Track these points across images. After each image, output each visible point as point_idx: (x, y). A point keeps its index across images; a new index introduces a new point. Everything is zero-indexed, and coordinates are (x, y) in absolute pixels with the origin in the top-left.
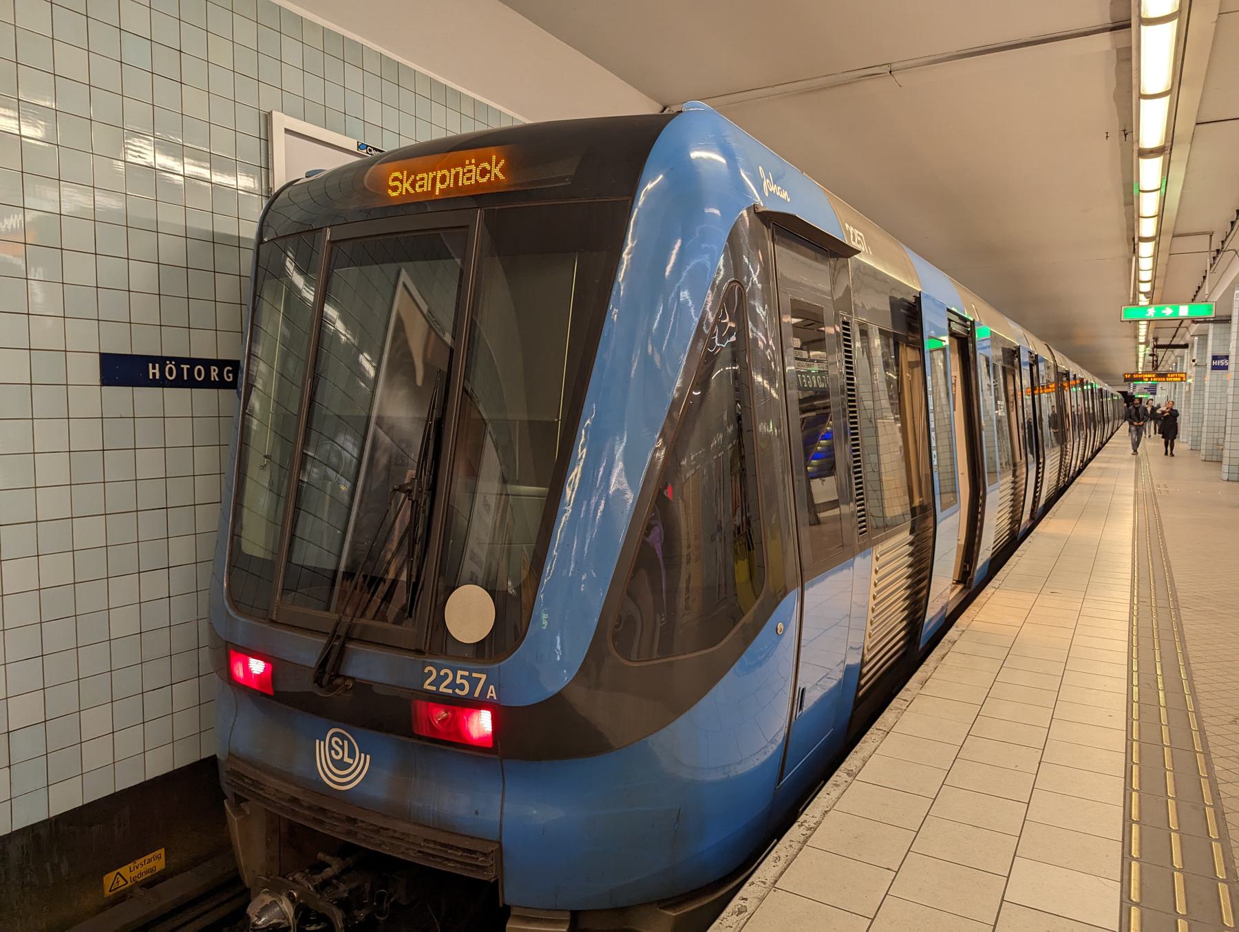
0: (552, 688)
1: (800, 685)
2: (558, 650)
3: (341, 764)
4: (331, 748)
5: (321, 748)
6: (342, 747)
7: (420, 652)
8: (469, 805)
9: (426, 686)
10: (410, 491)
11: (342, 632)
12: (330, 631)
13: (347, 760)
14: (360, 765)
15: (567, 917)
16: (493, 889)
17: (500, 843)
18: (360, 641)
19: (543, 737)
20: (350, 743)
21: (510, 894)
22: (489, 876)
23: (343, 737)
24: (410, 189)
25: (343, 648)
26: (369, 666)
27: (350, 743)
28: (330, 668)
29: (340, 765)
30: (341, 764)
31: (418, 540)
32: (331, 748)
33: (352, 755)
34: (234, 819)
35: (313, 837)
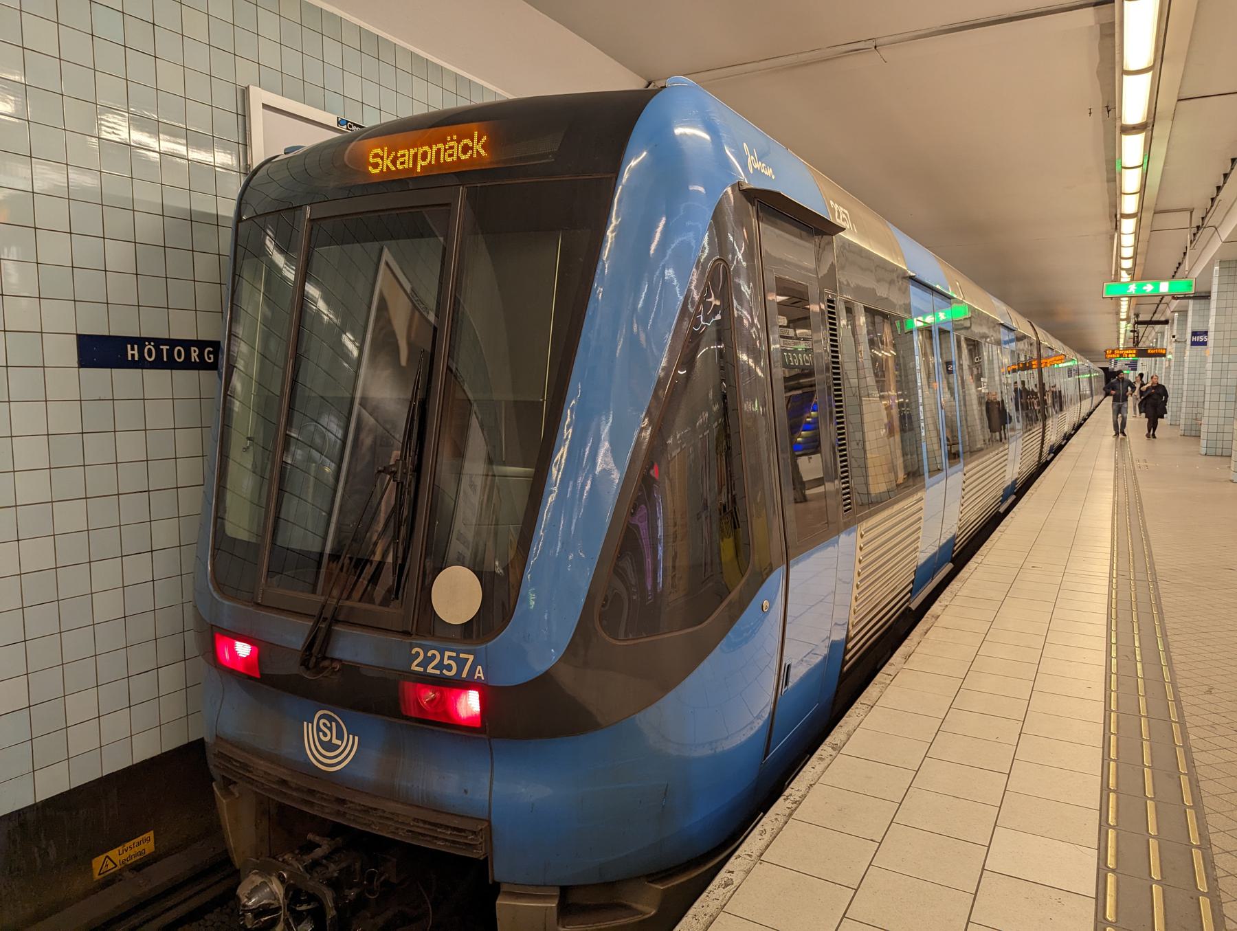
0: (540, 668)
1: (786, 661)
2: (545, 632)
3: (330, 746)
4: (319, 729)
5: (309, 730)
6: (330, 729)
7: (407, 633)
8: (456, 784)
9: (414, 667)
10: (395, 473)
11: (328, 614)
12: (316, 613)
13: (335, 741)
14: (349, 747)
15: (557, 892)
16: (483, 866)
17: (489, 822)
18: (347, 623)
19: (532, 716)
20: (338, 725)
21: (499, 872)
22: (478, 854)
23: (331, 719)
24: (393, 168)
25: (329, 632)
26: (355, 648)
27: (338, 725)
28: (317, 650)
29: (329, 746)
30: (330, 746)
31: (404, 521)
32: (319, 729)
33: (340, 736)
34: (223, 802)
35: (302, 818)
